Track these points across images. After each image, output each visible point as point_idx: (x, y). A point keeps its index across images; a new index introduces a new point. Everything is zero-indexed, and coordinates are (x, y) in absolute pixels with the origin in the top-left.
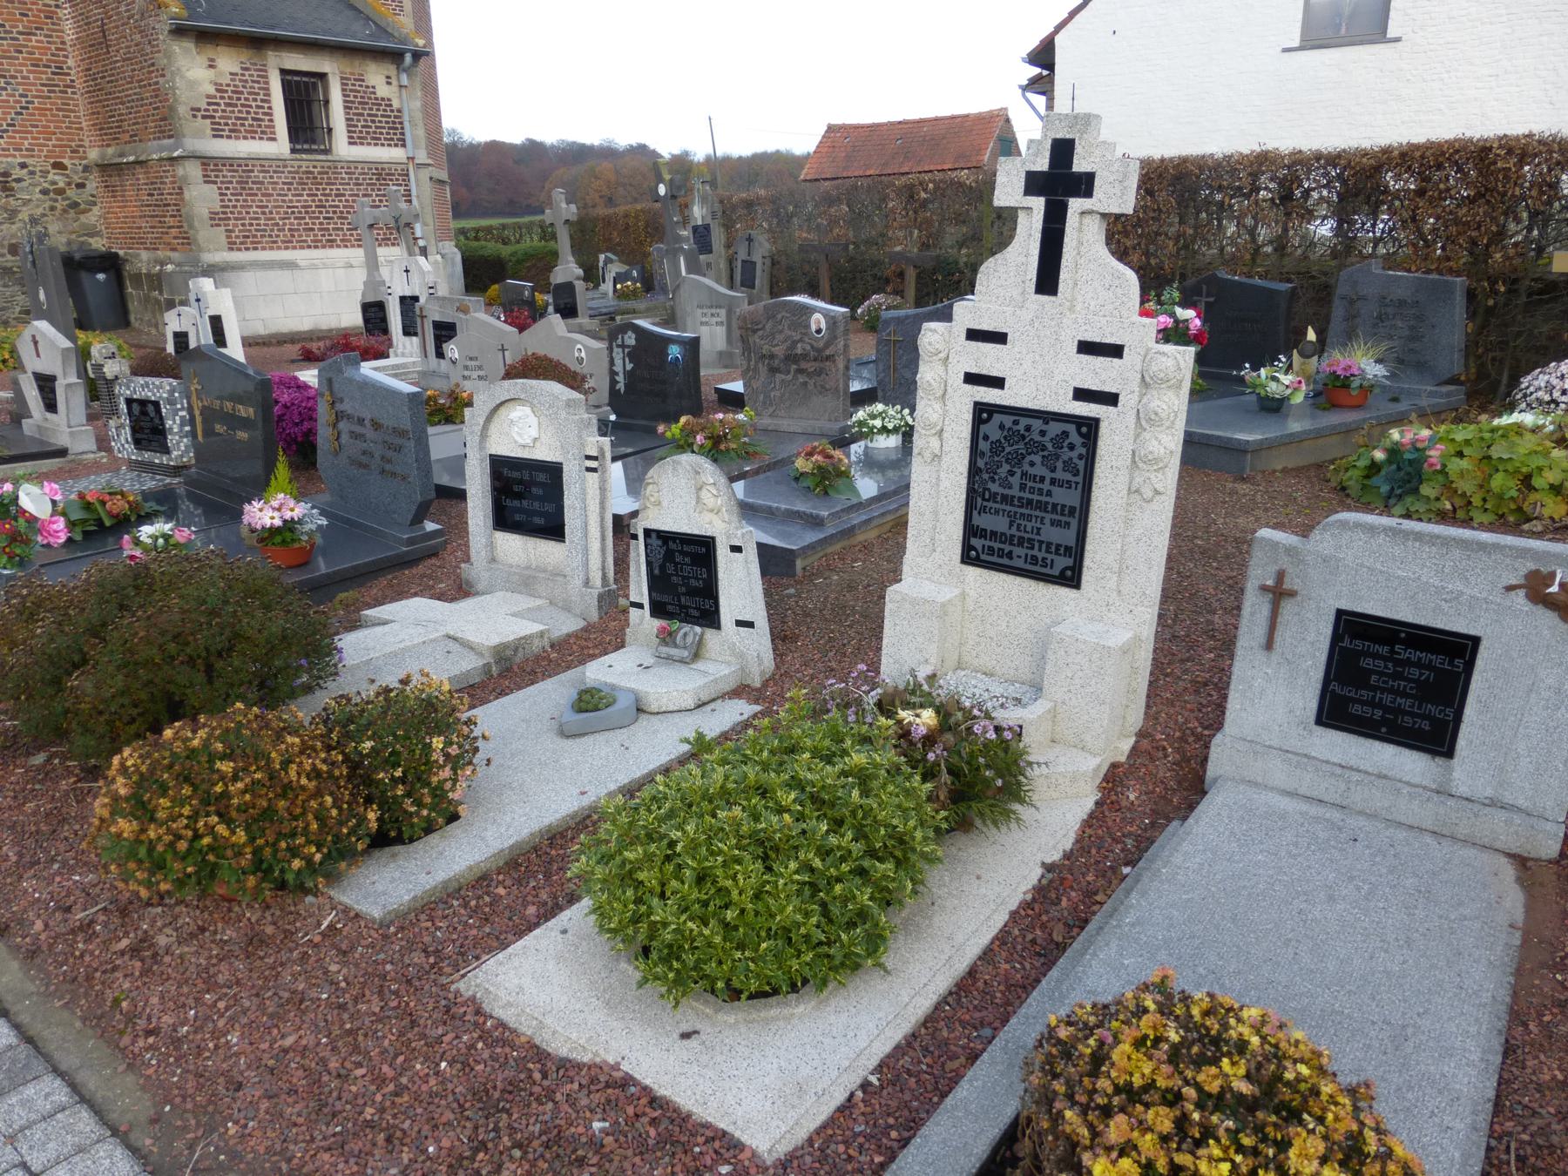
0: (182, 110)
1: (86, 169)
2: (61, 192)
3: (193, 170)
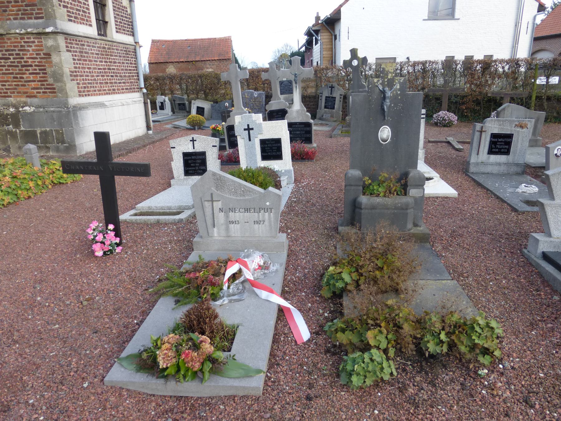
3: (61, 40)
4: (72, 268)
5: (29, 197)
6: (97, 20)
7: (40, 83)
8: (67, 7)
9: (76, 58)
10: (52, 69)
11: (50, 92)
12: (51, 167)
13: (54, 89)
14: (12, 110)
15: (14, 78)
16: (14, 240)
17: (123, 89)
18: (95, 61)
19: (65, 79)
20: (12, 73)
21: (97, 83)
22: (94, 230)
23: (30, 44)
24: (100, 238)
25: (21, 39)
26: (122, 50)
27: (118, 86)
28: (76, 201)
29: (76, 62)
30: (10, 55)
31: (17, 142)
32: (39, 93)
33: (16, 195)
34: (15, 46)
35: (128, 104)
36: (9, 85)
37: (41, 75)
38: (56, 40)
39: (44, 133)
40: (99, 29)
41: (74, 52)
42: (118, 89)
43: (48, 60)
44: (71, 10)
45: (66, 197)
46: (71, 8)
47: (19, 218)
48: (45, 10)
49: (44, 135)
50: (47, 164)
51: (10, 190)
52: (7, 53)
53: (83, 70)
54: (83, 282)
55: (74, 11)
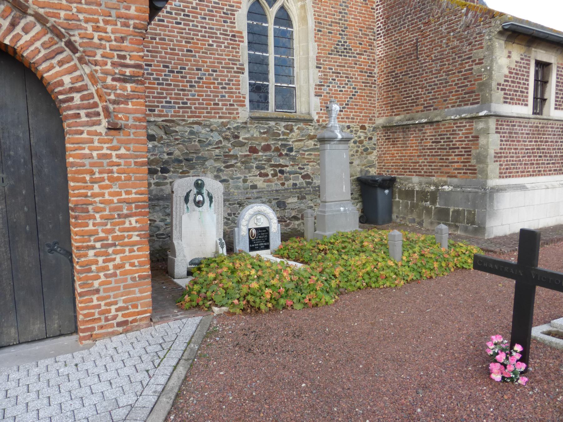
0: (494, 85)
1: (375, 129)
2: (361, 142)
3: (492, 123)
4: (460, 383)
5: (431, 277)
6: (535, 98)
7: (462, 164)
8: (504, 89)
9: (504, 139)
10: (478, 151)
11: (470, 173)
12: (458, 250)
13: (475, 170)
14: (432, 188)
15: (441, 159)
16: (409, 324)
17: (550, 171)
18: (524, 141)
19: (488, 160)
20: (440, 155)
21: (521, 164)
22: (495, 344)
23: (461, 128)
24: (501, 358)
25: (454, 124)
26: (557, 128)
27: (545, 167)
28: (476, 293)
29: (502, 143)
30: (441, 139)
31: (430, 218)
32: (460, 173)
33: (420, 273)
34: (447, 131)
35: (554, 187)
36: (435, 166)
37: (466, 157)
38: (487, 123)
39: (457, 212)
40: (535, 107)
41: (503, 133)
42: (544, 171)
43: (475, 142)
44: (508, 92)
45: (467, 287)
46: (509, 90)
47: (418, 299)
48: (482, 96)
49: (456, 214)
50: (453, 245)
51: (415, 267)
52: (439, 137)
53: (508, 152)
54: (471, 410)
55: (511, 93)
